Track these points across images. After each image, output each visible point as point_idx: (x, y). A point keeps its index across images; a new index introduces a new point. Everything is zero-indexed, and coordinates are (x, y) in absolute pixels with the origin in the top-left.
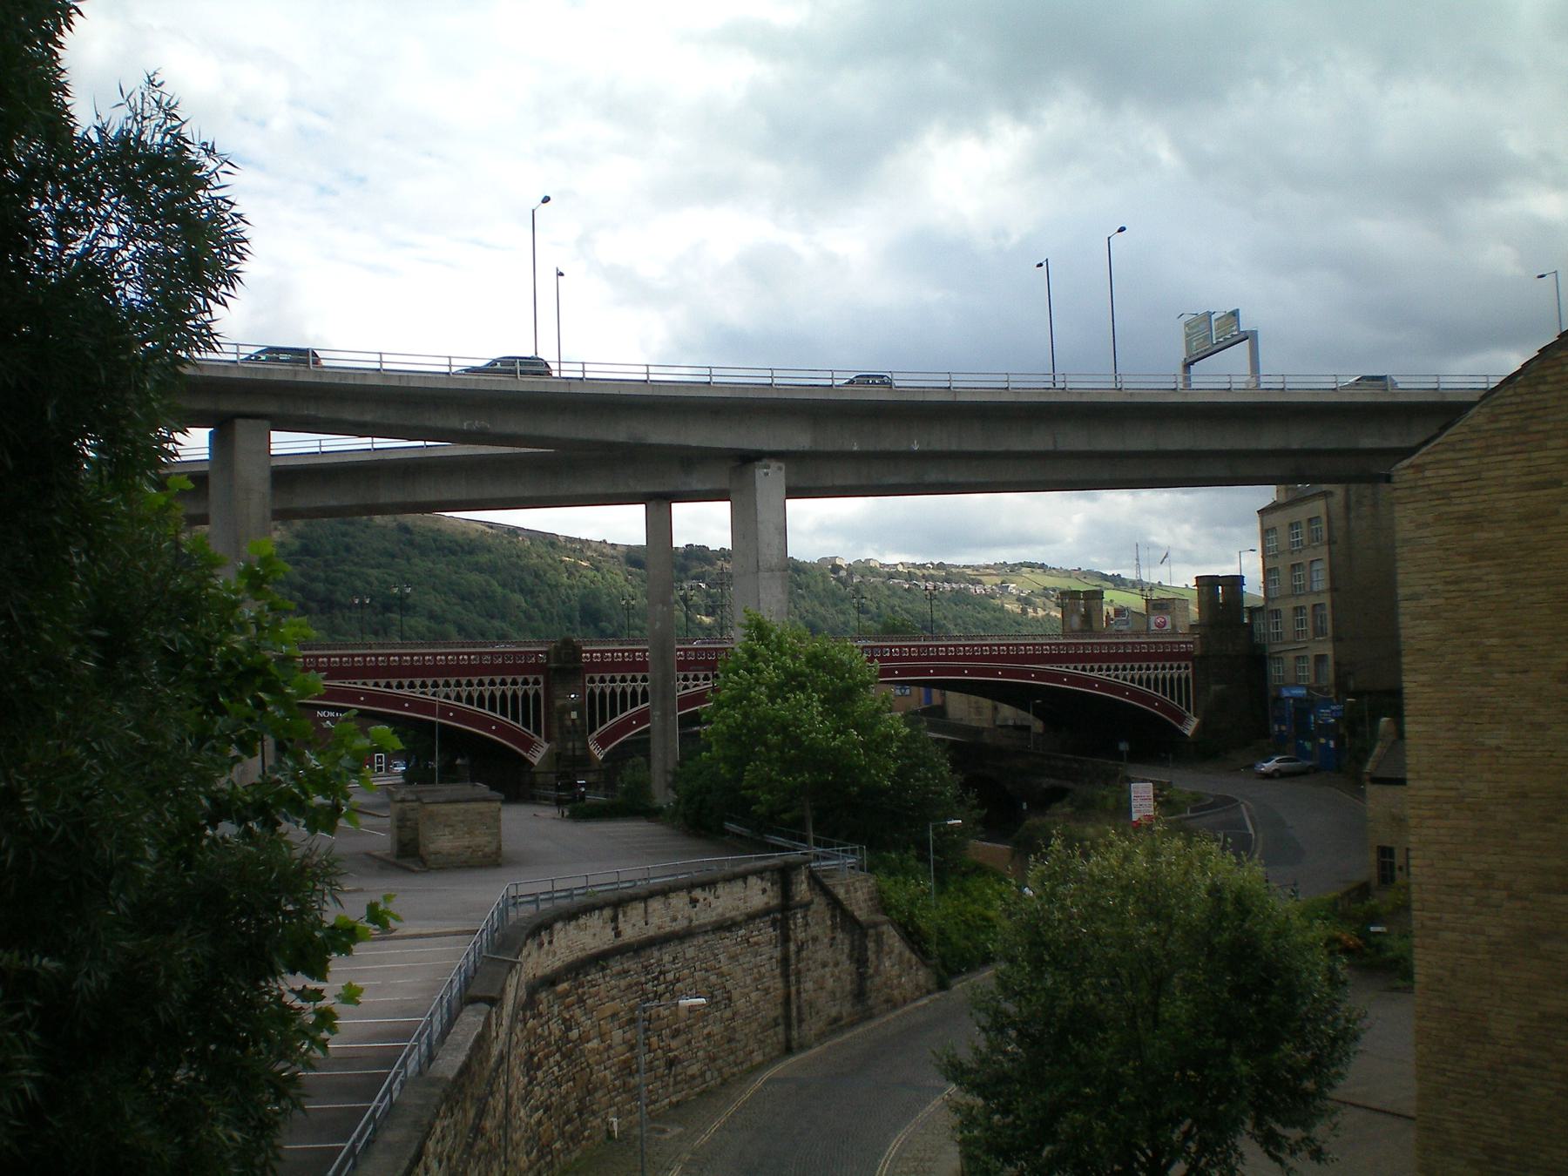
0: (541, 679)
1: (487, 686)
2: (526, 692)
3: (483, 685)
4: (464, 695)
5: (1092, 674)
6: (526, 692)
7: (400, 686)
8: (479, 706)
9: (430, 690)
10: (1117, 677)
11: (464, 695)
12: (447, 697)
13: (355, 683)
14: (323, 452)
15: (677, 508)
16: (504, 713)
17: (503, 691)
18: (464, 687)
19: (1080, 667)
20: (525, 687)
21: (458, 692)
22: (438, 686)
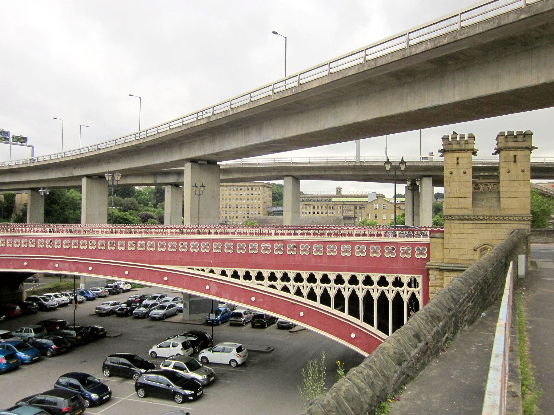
0: (420, 279)
1: (305, 282)
2: (398, 296)
3: (401, 284)
4: (318, 293)
5: (247, 283)
6: (398, 296)
7: (247, 276)
8: (322, 302)
9: (279, 284)
10: (285, 289)
11: (318, 293)
12: (299, 293)
13: (203, 270)
14: (485, 175)
15: (301, 181)
16: (369, 319)
17: (325, 290)
18: (318, 282)
19: (229, 271)
20: (383, 288)
21: (312, 289)
22: (288, 280)
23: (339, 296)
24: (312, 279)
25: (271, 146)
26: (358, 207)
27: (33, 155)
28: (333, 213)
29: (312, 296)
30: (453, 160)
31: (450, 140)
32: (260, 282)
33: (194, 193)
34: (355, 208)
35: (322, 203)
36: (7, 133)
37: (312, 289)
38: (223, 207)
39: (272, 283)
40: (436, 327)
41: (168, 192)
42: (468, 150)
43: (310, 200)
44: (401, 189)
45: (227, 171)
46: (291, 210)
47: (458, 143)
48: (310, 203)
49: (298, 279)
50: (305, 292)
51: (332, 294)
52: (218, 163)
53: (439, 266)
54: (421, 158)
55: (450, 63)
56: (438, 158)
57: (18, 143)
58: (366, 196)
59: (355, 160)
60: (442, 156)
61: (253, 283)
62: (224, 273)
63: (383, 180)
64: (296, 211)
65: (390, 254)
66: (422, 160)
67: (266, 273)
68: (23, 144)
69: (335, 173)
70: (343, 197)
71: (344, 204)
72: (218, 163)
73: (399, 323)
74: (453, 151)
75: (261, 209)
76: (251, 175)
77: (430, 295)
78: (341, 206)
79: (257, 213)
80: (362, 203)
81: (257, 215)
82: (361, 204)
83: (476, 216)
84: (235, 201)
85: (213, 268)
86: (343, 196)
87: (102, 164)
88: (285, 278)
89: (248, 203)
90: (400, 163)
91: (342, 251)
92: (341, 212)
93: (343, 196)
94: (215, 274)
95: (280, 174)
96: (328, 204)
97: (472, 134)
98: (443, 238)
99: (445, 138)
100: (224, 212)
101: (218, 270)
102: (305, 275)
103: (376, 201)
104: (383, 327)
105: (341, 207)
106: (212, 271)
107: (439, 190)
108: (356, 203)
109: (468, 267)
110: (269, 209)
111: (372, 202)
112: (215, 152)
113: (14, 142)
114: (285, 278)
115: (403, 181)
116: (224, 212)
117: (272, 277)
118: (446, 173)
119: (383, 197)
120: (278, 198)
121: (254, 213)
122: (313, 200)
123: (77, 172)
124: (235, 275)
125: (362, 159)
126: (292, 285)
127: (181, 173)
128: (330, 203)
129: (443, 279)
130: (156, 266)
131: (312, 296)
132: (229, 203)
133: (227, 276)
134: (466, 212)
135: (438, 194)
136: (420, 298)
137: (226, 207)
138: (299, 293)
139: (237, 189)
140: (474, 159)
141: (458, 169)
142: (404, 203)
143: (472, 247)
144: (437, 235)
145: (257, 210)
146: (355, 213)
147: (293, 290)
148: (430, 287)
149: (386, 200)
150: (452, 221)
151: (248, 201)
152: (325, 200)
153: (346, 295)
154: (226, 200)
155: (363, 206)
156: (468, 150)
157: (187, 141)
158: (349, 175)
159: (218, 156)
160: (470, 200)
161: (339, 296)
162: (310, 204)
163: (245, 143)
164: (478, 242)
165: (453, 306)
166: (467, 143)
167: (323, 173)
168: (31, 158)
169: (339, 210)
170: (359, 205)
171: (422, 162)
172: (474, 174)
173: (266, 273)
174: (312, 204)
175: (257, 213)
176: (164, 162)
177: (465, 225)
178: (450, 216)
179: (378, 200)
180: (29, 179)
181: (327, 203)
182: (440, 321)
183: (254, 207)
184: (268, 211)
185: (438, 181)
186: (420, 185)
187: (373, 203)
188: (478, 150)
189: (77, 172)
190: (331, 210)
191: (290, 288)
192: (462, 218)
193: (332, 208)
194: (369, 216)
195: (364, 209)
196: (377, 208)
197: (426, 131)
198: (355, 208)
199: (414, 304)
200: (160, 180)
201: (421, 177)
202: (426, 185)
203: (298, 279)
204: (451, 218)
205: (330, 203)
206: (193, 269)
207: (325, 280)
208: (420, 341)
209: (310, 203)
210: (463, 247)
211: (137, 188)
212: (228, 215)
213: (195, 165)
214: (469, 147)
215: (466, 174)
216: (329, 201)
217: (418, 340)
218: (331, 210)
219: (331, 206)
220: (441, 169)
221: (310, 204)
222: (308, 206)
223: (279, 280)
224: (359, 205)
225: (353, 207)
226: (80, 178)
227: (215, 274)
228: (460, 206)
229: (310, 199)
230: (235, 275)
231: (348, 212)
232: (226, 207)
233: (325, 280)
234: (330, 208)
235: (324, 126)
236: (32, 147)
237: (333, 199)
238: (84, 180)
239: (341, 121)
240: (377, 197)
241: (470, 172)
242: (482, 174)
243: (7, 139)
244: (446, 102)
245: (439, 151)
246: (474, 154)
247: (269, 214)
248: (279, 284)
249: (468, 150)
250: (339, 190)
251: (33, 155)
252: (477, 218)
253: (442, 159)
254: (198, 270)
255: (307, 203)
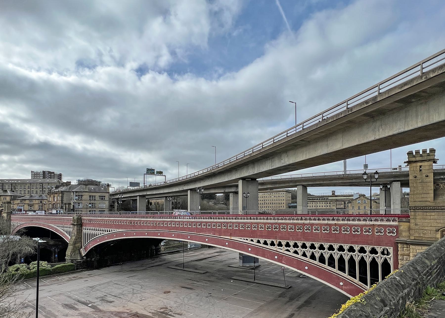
0: (391, 250)
2: (374, 260)
4: (317, 256)
5: (272, 248)
6: (374, 260)
7: (272, 244)
10: (296, 252)
11: (317, 256)
12: (304, 255)
13: (247, 240)
19: (262, 241)
21: (313, 253)
23: (331, 258)
24: (313, 247)
25: (287, 168)
26: (346, 202)
27: (165, 180)
28: (330, 206)
29: (313, 257)
30: (416, 168)
31: (414, 154)
32: (280, 247)
33: (243, 197)
34: (345, 203)
35: (320, 200)
36: (154, 170)
37: (313, 253)
38: (260, 204)
39: (288, 248)
40: (401, 294)
41: (231, 196)
42: (429, 160)
43: (315, 199)
44: (376, 190)
45: (263, 184)
46: (301, 205)
47: (421, 156)
48: (315, 201)
49: (304, 246)
50: (308, 254)
51: (327, 256)
52: (257, 180)
53: (406, 241)
54: (392, 169)
55: (413, 100)
56: (406, 168)
57: (159, 175)
58: (352, 196)
59: (343, 174)
60: (408, 165)
61: (275, 248)
62: (259, 242)
63: (363, 185)
64: (305, 205)
65: (367, 233)
66: (392, 171)
67: (284, 243)
68: (161, 175)
69: (330, 182)
70: (336, 197)
71: (337, 200)
72: (257, 180)
73: (374, 280)
74: (416, 162)
75: (284, 205)
76: (277, 186)
77: (399, 261)
78: (335, 202)
79: (282, 207)
80: (349, 200)
81: (282, 208)
82: (349, 201)
83: (437, 206)
84: (270, 200)
85: (253, 239)
86: (336, 196)
87: (197, 183)
88: (296, 246)
89: (277, 202)
90: (374, 174)
91: (332, 230)
92: (335, 206)
93: (336, 196)
94: (254, 242)
95: (294, 184)
96: (326, 201)
97: (433, 149)
98: (410, 222)
99: (410, 154)
100: (263, 207)
101: (255, 240)
102: (308, 244)
103: (359, 198)
104: (363, 280)
105: (335, 203)
106: (252, 240)
107: (406, 190)
108: (345, 200)
109: (431, 245)
110: (289, 205)
111: (356, 199)
112: (255, 173)
113: (157, 174)
114: (296, 246)
115: (377, 185)
116: (263, 207)
117: (288, 245)
118: (411, 177)
119: (364, 196)
120: (294, 197)
121: (280, 207)
122: (313, 199)
123: (185, 188)
124: (265, 243)
125: (348, 173)
126: (300, 250)
127: (237, 186)
128: (327, 200)
129: (409, 250)
130: (221, 237)
131: (313, 257)
132: (266, 202)
133: (261, 243)
134: (428, 204)
135: (405, 193)
136: (391, 262)
137: (264, 204)
138: (304, 255)
139: (272, 194)
140: (435, 167)
141: (421, 174)
142: (379, 199)
143: (434, 229)
144: (404, 220)
145: (282, 205)
146: (345, 206)
147: (301, 253)
148: (399, 256)
149: (366, 198)
150: (417, 211)
151: (277, 200)
152: (323, 198)
153: (336, 257)
154: (264, 200)
155: (350, 201)
156: (429, 160)
157: (240, 168)
158: (340, 183)
159: (256, 176)
160: (432, 195)
161: (331, 258)
162: (315, 201)
163: (272, 167)
164: (440, 225)
165: (417, 276)
166: (428, 155)
167: (322, 182)
168: (164, 181)
169: (334, 204)
170: (348, 201)
171: (392, 172)
172: (436, 178)
173: (284, 243)
174: (316, 201)
175: (282, 207)
176: (228, 180)
177: (427, 214)
178: (415, 207)
179: (360, 198)
180: (164, 192)
181: (326, 200)
182: (404, 288)
183: (280, 203)
184: (289, 206)
185: (405, 184)
186: (390, 187)
187: (357, 200)
188: (438, 160)
189: (185, 188)
190: (328, 205)
191: (299, 252)
192: (424, 209)
193: (329, 203)
194: (354, 208)
195: (350, 203)
196: (359, 203)
197: (395, 150)
198: (345, 203)
199: (386, 265)
200: (227, 190)
201: (391, 182)
202: (396, 186)
203: (304, 246)
204: (416, 208)
205: (327, 200)
206: (242, 239)
207: (322, 247)
208: (386, 306)
209: (315, 201)
210: (426, 228)
211: (218, 195)
212: (265, 208)
213: (245, 181)
214: (431, 157)
215: (428, 177)
216: (327, 199)
217: (384, 305)
218: (328, 205)
219: (329, 202)
220: (408, 175)
221: (315, 201)
222: (314, 203)
223: (292, 247)
224: (348, 201)
225: (343, 203)
226: (186, 191)
227: (254, 242)
228: (424, 200)
229: (317, 198)
230: (265, 243)
231: (340, 205)
232: (264, 204)
233: (322, 247)
234: (327, 203)
235: (320, 153)
236: (165, 176)
237: (329, 198)
238: (189, 192)
239: (331, 149)
240: (359, 196)
241: (432, 175)
242: (442, 177)
243: (154, 173)
244: (411, 128)
245: (405, 162)
246: (435, 162)
247: (290, 207)
248: (292, 249)
249: (430, 160)
250: (333, 192)
251: (165, 180)
252: (438, 208)
253: (407, 169)
254: (244, 239)
255: (312, 201)
